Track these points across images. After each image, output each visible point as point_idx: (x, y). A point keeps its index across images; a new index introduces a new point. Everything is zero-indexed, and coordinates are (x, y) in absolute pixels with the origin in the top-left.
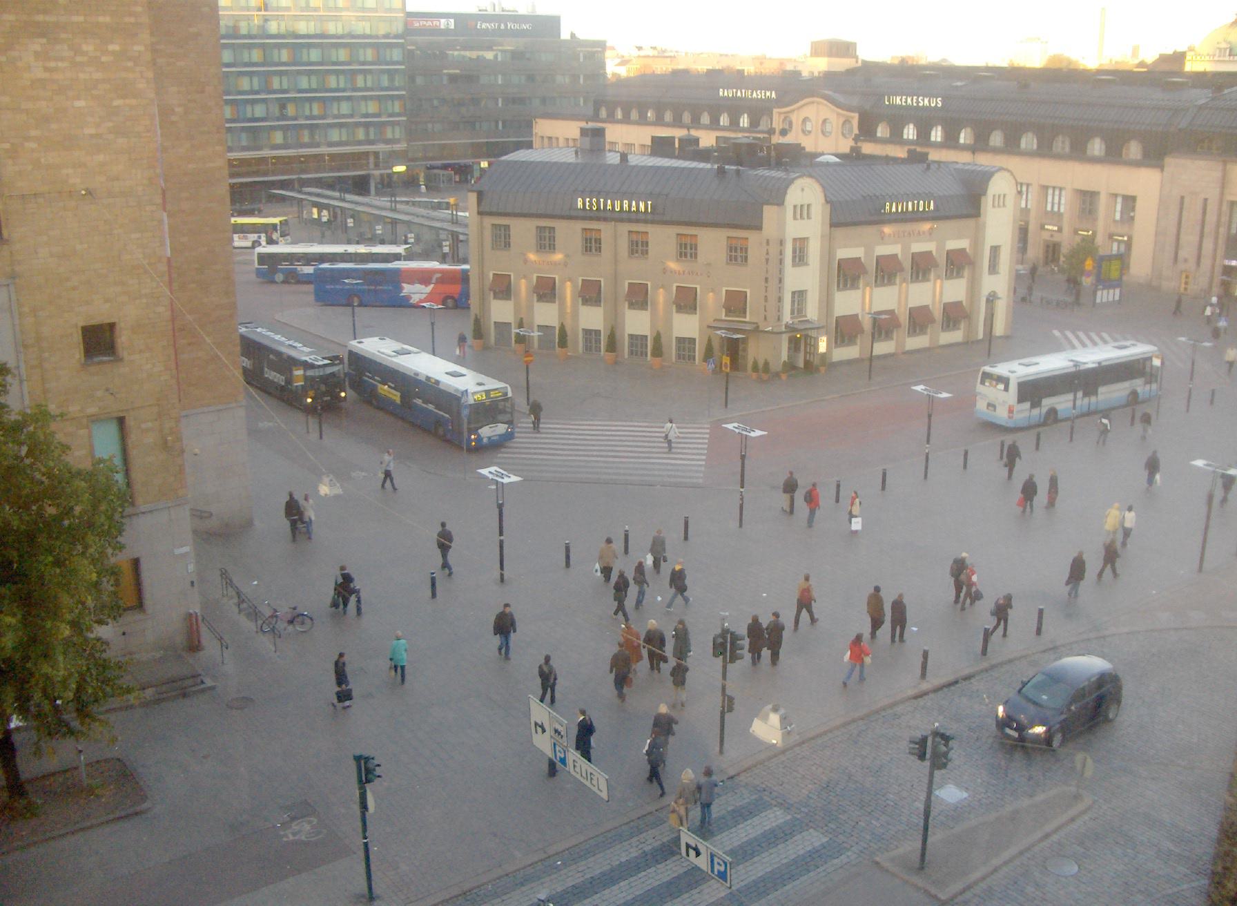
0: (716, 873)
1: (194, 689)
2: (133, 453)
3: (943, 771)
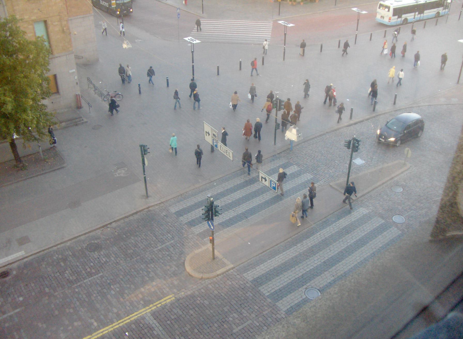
0: (272, 187)
1: (79, 122)
2: (51, 34)
3: (356, 153)
